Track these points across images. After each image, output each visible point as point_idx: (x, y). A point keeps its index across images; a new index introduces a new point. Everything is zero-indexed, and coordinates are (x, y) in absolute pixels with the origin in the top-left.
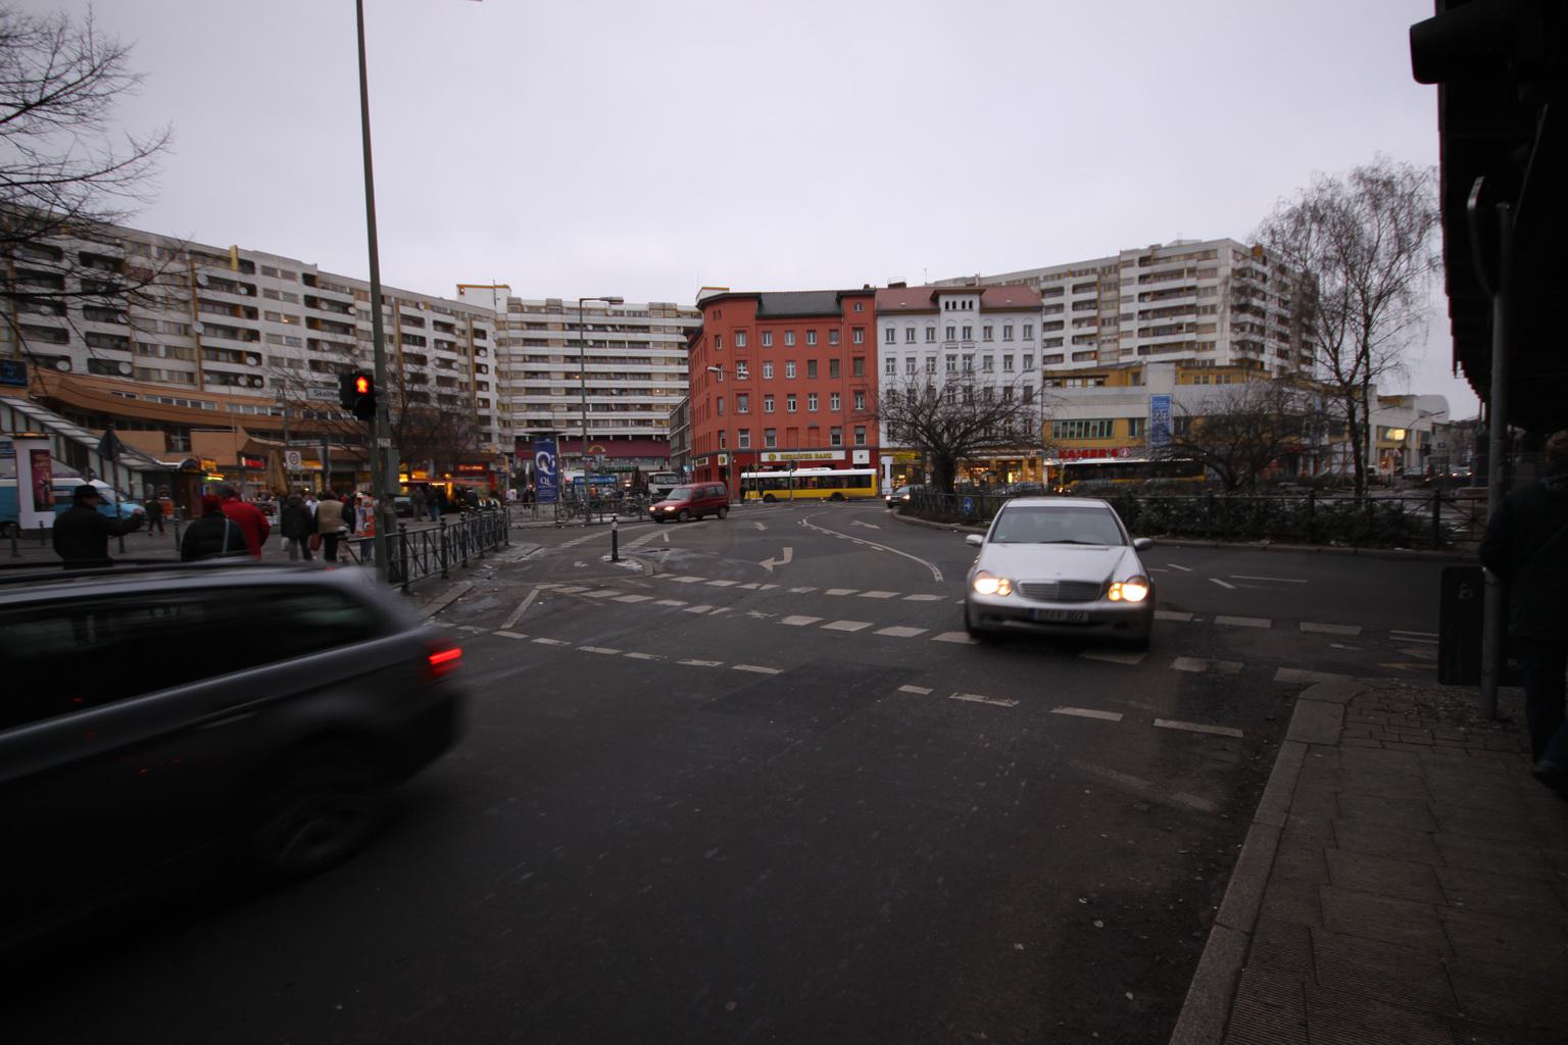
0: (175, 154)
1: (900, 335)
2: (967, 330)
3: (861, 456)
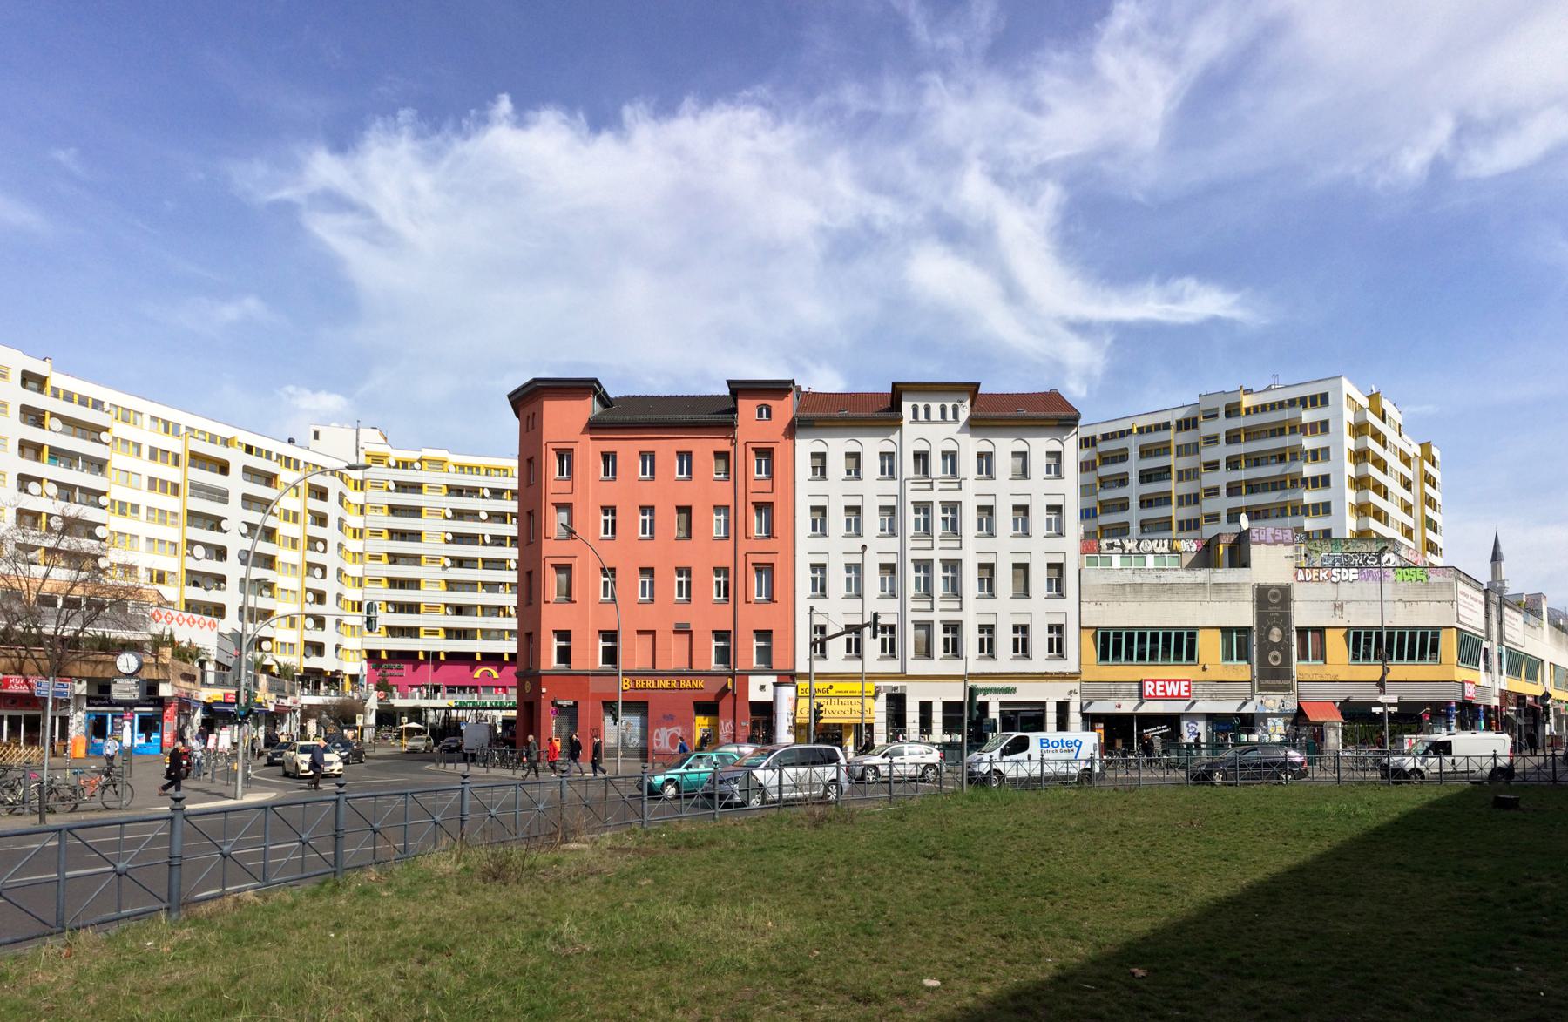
0: (639, 632)
1: (837, 465)
2: (950, 457)
3: (762, 687)
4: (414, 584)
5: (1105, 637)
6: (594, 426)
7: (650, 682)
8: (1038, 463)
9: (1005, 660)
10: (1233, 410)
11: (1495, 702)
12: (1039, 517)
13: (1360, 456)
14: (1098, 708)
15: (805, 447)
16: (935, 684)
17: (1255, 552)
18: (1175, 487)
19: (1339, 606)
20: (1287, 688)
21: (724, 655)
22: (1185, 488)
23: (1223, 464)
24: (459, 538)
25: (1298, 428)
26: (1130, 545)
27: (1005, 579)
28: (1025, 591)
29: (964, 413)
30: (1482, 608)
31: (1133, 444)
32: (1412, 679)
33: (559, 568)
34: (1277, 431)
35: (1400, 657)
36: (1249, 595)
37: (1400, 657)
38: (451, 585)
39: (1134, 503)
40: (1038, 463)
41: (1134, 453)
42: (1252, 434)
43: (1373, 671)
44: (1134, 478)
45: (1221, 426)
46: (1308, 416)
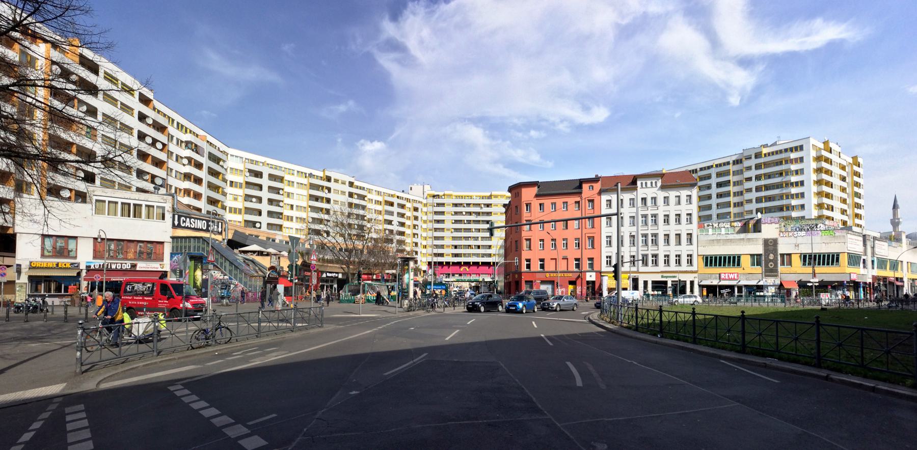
4: (442, 238)
5: (707, 258)
6: (537, 196)
7: (555, 275)
8: (684, 199)
9: (673, 267)
10: (758, 155)
11: (871, 281)
12: (684, 218)
13: (819, 170)
14: (704, 283)
15: (605, 198)
16: (649, 274)
17: (763, 226)
18: (732, 189)
19: (797, 246)
20: (776, 276)
21: (578, 266)
22: (737, 189)
23: (754, 178)
24: (456, 222)
25: (788, 161)
26: (716, 225)
27: (673, 239)
28: (679, 243)
29: (659, 184)
30: (862, 243)
31: (713, 172)
32: (826, 273)
33: (527, 240)
34: (779, 163)
35: (819, 264)
36: (761, 242)
37: (819, 264)
38: (454, 238)
39: (714, 196)
40: (684, 199)
41: (714, 175)
42: (767, 165)
43: (809, 269)
44: (714, 186)
45: (753, 162)
46: (793, 156)
